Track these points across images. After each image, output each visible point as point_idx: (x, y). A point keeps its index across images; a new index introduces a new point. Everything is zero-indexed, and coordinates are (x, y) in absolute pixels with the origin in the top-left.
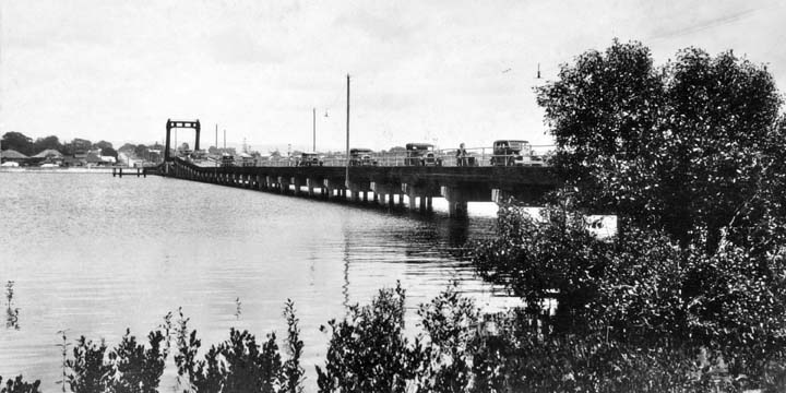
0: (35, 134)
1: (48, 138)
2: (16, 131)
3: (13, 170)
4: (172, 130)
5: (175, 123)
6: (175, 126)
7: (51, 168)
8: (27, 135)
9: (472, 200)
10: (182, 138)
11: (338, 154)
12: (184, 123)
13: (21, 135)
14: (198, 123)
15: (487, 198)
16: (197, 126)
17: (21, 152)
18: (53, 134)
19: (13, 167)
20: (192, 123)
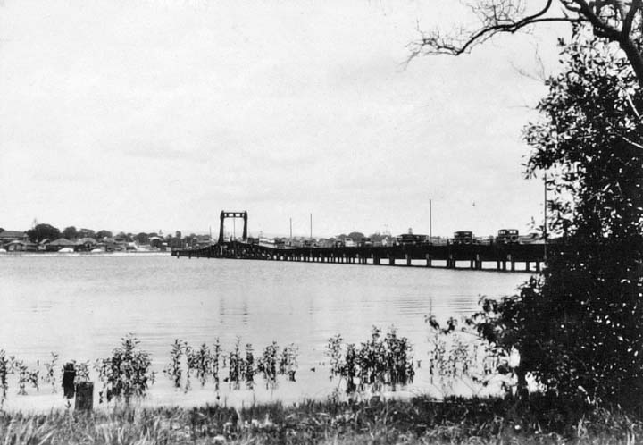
0: (484, 232)
1: (56, 229)
2: (46, 223)
3: (70, 255)
4: (226, 220)
5: (228, 214)
6: (228, 216)
7: (99, 253)
8: (55, 227)
9: (434, 259)
10: (234, 230)
11: (207, 237)
12: (234, 214)
13: (50, 226)
14: (246, 214)
15: (404, 258)
16: (245, 216)
17: (539, 245)
18: (69, 226)
19: (69, 252)
20: (241, 214)
